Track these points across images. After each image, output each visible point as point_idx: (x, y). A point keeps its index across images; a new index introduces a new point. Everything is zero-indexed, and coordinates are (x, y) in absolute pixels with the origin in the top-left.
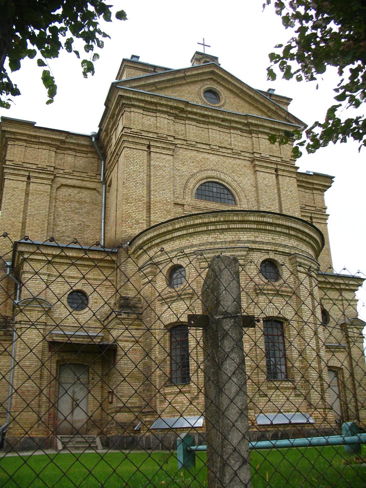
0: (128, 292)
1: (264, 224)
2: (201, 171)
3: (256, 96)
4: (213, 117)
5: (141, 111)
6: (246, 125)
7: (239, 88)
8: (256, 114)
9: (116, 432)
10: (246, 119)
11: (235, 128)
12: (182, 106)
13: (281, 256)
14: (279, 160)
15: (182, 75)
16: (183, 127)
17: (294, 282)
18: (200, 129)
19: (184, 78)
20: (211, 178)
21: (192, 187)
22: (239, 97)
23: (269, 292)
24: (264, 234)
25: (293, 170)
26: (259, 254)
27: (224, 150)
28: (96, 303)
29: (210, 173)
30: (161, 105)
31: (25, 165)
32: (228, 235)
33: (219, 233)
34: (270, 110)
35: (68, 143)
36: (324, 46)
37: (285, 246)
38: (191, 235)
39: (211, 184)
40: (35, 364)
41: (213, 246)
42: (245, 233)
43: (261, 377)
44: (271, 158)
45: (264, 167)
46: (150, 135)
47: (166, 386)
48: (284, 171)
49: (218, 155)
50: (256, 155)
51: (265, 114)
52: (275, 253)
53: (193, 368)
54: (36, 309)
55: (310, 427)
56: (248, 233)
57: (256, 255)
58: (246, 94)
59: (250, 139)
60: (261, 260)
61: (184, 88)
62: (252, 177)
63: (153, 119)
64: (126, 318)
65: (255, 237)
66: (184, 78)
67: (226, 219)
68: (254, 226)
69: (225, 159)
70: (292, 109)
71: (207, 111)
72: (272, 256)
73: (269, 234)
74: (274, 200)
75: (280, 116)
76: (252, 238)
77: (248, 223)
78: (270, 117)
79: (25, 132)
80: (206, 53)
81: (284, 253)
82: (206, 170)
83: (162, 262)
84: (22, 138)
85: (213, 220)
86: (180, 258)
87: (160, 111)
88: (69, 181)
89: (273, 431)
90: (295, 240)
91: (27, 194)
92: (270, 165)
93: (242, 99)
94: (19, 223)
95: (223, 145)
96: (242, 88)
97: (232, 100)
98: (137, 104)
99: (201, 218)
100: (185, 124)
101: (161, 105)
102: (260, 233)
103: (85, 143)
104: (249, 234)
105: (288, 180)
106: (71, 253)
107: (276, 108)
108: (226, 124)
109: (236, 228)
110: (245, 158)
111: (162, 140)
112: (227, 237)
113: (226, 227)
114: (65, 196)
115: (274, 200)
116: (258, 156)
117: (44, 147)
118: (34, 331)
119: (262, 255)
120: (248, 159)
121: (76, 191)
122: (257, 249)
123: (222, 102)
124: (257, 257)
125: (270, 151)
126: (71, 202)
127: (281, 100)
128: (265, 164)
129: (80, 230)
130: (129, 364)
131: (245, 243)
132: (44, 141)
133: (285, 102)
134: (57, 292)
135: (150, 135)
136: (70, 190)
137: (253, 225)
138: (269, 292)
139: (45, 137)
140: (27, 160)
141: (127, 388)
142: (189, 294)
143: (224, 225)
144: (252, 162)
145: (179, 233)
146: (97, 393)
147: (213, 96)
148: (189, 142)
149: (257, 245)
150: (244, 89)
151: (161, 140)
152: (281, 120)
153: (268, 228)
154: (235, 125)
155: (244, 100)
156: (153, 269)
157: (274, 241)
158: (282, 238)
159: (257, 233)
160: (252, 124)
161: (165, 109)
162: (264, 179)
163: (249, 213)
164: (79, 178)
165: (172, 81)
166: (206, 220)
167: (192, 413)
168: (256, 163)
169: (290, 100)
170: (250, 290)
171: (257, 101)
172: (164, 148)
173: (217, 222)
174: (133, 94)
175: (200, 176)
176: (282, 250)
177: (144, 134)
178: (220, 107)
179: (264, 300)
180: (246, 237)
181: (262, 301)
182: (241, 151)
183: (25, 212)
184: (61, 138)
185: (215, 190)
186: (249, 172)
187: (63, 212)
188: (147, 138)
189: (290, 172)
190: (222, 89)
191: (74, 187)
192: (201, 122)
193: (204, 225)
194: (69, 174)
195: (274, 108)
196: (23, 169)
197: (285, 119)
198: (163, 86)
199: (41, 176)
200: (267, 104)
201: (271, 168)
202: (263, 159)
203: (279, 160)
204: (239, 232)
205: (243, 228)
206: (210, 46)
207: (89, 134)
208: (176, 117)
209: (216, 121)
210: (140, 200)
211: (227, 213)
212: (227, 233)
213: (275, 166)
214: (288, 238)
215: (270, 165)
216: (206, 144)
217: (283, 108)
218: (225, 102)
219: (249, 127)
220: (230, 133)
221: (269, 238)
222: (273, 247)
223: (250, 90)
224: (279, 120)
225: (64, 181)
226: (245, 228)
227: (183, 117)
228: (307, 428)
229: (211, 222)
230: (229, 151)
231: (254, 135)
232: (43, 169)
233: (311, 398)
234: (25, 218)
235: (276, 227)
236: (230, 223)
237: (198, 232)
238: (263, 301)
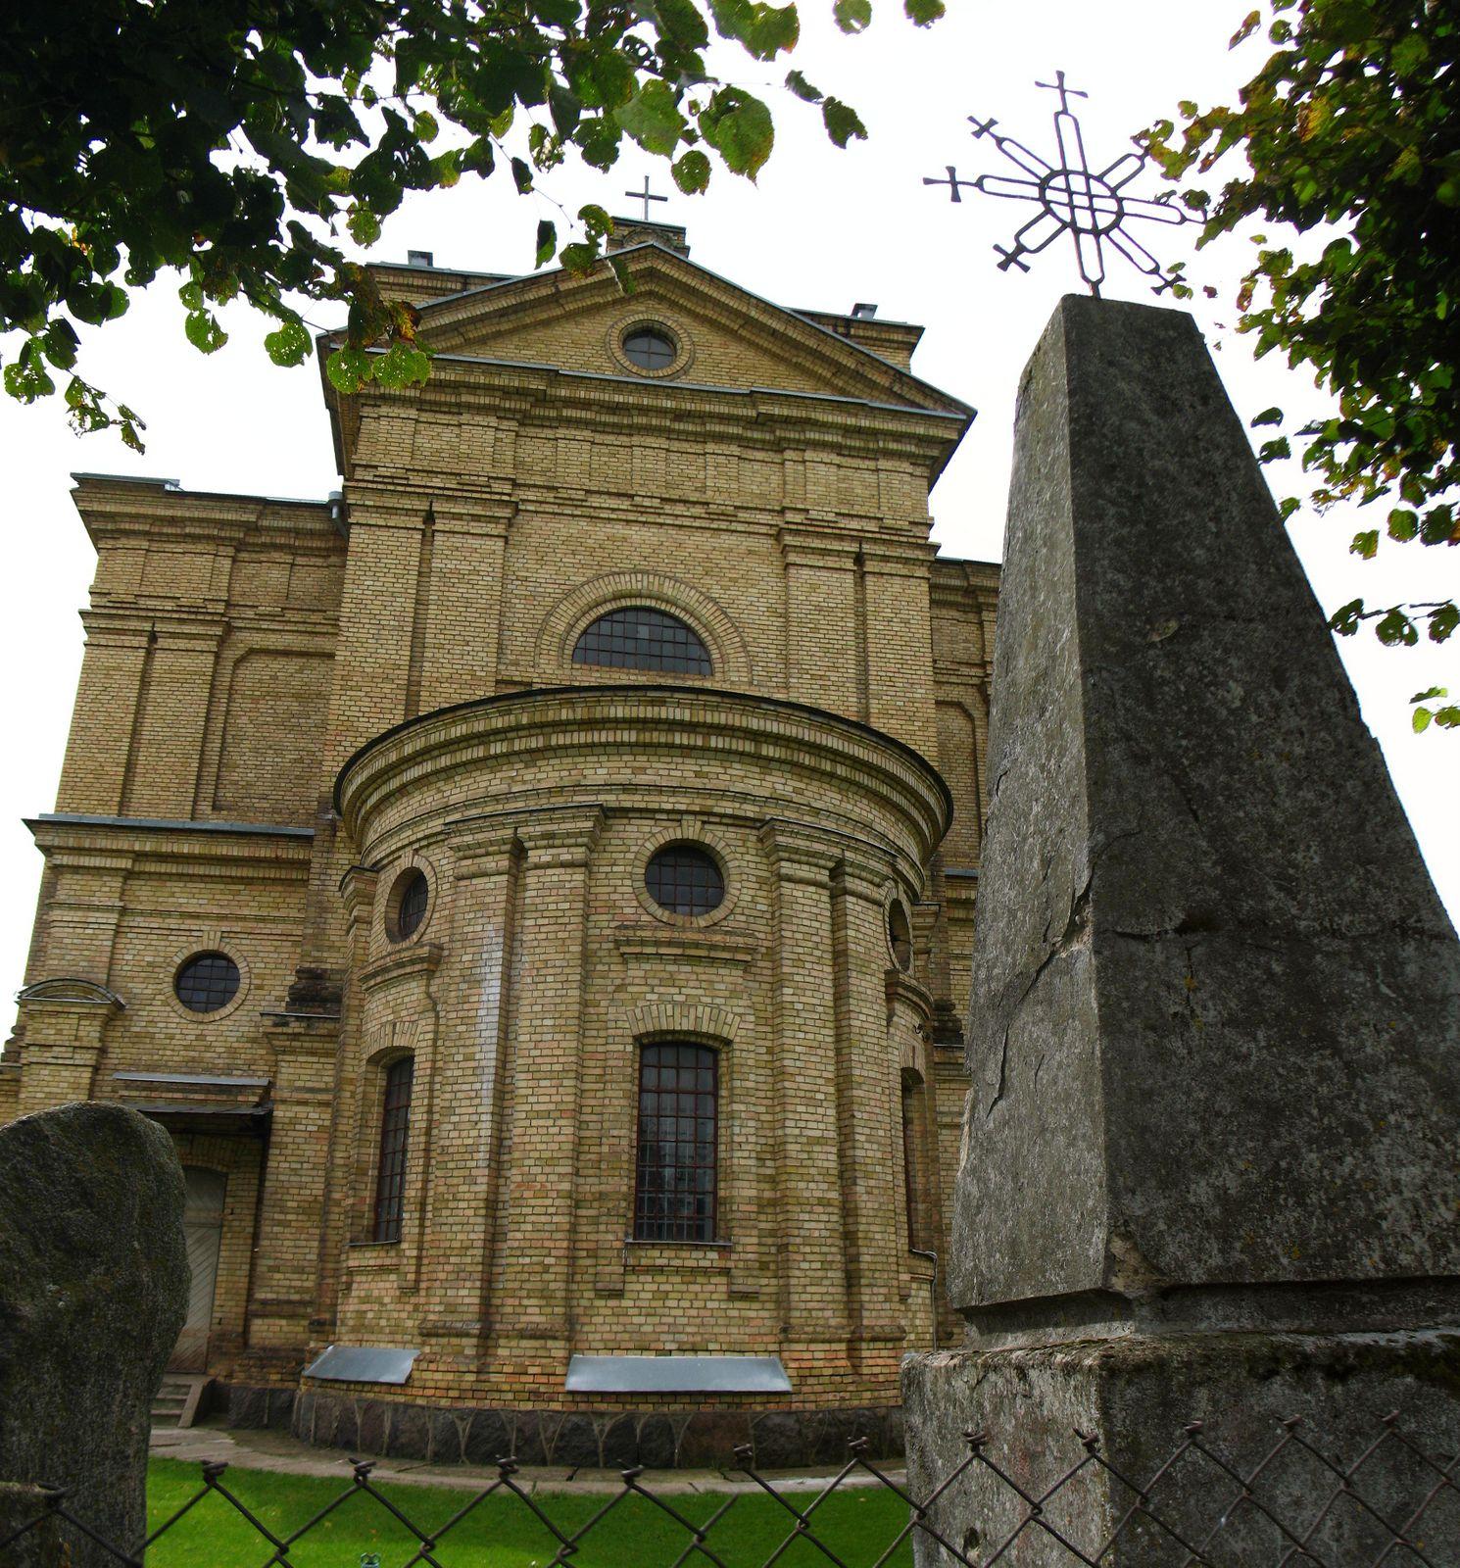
0: (325, 955)
1: (666, 727)
2: (598, 577)
3: (790, 333)
4: (644, 410)
5: (413, 413)
6: (756, 422)
7: (737, 313)
8: (795, 386)
9: (242, 1375)
10: (754, 406)
11: (721, 438)
12: (536, 384)
13: (731, 829)
14: (872, 526)
15: (544, 292)
16: (547, 449)
17: (768, 916)
18: (605, 450)
19: (556, 298)
20: (640, 596)
21: (561, 628)
22: (741, 339)
23: (662, 951)
24: (669, 760)
25: (920, 554)
26: (646, 826)
27: (679, 509)
28: (260, 987)
29: (626, 583)
30: (473, 388)
31: (142, 602)
32: (550, 768)
33: (522, 765)
34: (839, 369)
35: (268, 529)
36: (1390, 223)
37: (745, 797)
38: (448, 773)
39: (631, 617)
41: (500, 807)
42: (604, 758)
43: (607, 1232)
44: (843, 523)
45: (814, 551)
46: (437, 482)
47: (355, 1246)
48: (885, 559)
49: (661, 524)
50: (790, 516)
51: (827, 383)
52: (704, 822)
53: (413, 1193)
54: (73, 1010)
55: (772, 1406)
56: (612, 758)
57: (635, 829)
58: (763, 328)
59: (776, 468)
60: (651, 847)
61: (558, 331)
62: (773, 583)
63: (448, 434)
64: (300, 1034)
65: (635, 771)
66: (556, 298)
67: (538, 718)
68: (629, 736)
69: (681, 536)
70: (923, 365)
71: (621, 392)
72: (691, 830)
73: (687, 761)
74: (842, 652)
75: (873, 385)
76: (625, 776)
77: (607, 725)
78: (842, 392)
79: (142, 511)
80: (652, 219)
81: (738, 821)
82: (614, 574)
83: (385, 862)
84: (137, 527)
85: (499, 723)
86: (421, 848)
87: (469, 407)
88: (273, 637)
89: (616, 1414)
90: (789, 776)
91: (145, 682)
92: (836, 546)
93: (751, 344)
94: (118, 765)
95: (674, 494)
96: (744, 310)
98: (893, 446)
99: (465, 719)
100: (556, 439)
101: (473, 388)
102: (652, 758)
103: (318, 526)
104: (615, 762)
105: (897, 589)
106: (236, 848)
107: (859, 362)
108: (690, 428)
109: (572, 746)
110: (751, 528)
111: (469, 495)
112: (544, 775)
114: (260, 681)
115: (842, 652)
116: (799, 518)
117: (200, 548)
118: (64, 1073)
119: (655, 830)
120: (764, 530)
121: (293, 664)
122: (640, 810)
123: (682, 360)
124: (641, 835)
125: (841, 502)
126: (277, 697)
127: (884, 336)
128: (817, 543)
129: (297, 777)
130: (303, 1172)
131: (598, 793)
132: (198, 531)
133: (897, 342)
134: (147, 959)
135: (437, 482)
136: (276, 665)
137: (626, 733)
138: (662, 951)
139: (201, 520)
140: (151, 589)
141: (292, 1243)
142: (422, 960)
143: (534, 739)
144: (778, 536)
145: (415, 772)
146: (239, 1254)
147: (657, 346)
148: (563, 494)
149: (639, 798)
150: (753, 313)
151: (475, 495)
152: (886, 402)
153: (679, 739)
154: (718, 428)
155: (758, 347)
156: (362, 886)
157: (698, 783)
158: (737, 769)
159: (645, 758)
161: (485, 400)
162: (814, 588)
163: (609, 695)
164: (302, 628)
165: (516, 312)
166: (480, 726)
168: (788, 539)
169: (917, 331)
170: (605, 946)
171: (797, 346)
172: (476, 518)
173: (511, 729)
175: (591, 594)
176: (729, 811)
177: (415, 479)
178: (672, 377)
179: (645, 978)
180: (605, 771)
181: (637, 981)
182: (736, 507)
183: (135, 732)
184: (245, 517)
185: (644, 632)
186: (765, 569)
187: (250, 730)
188: (421, 490)
189: (906, 561)
190: (685, 320)
191: (286, 653)
192: (758, 446)
193: (476, 741)
194: (272, 618)
195: (851, 363)
196: (134, 613)
197: (890, 392)
198: (485, 330)
199: (186, 629)
200: (827, 351)
201: (839, 553)
202: (814, 528)
203: (872, 526)
204: (582, 759)
205: (593, 745)
206: (628, 194)
207: (324, 498)
208: (525, 420)
209: (654, 422)
210: (386, 679)
211: (539, 698)
212: (545, 762)
213: (854, 547)
214: (758, 770)
215: (836, 546)
216: (618, 495)
217: (880, 358)
218: (693, 360)
220: (705, 454)
221: (686, 774)
222: (697, 801)
223: (772, 316)
224: (881, 401)
225: (257, 640)
227: (549, 418)
228: (759, 1408)
229: (496, 732)
230: (698, 510)
231: (789, 454)
232: (194, 610)
233: (793, 1305)
234: (132, 751)
235: (709, 734)
236: (550, 730)
237: (464, 764)
238: (643, 982)
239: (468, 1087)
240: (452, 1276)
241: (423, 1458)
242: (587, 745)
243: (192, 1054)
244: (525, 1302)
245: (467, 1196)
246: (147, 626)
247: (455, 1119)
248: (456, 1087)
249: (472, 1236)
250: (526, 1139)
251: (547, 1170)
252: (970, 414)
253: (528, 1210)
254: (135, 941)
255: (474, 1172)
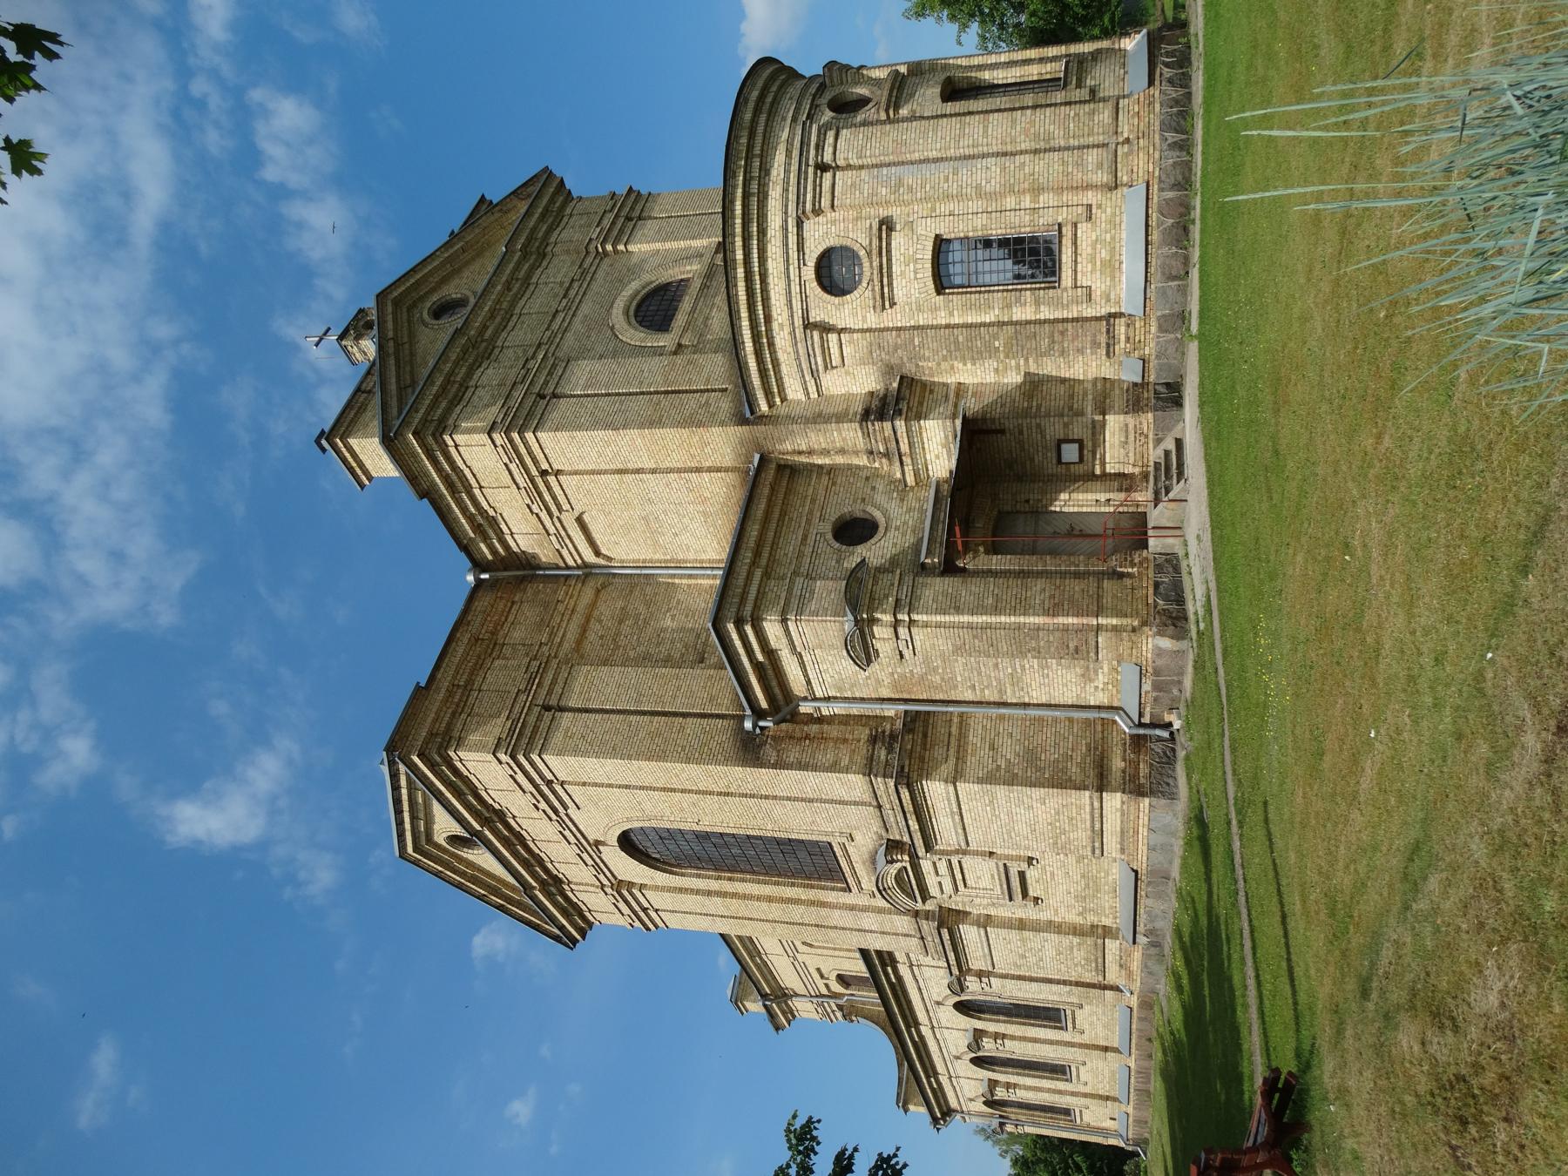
40: (991, 589)
68: (763, 118)
78: (529, 196)
97: (464, 281)
100: (502, 347)
113: (758, 160)
126: (618, 634)
129: (687, 616)
160: (525, 246)
167: (1118, 219)
172: (550, 374)
174: (417, 412)
219: (536, 239)
226: (765, 130)
230: (576, 285)
239: (965, 177)
240: (1080, 168)
241: (1191, 162)
242: (764, 136)
243: (909, 532)
244: (1096, 122)
245: (1032, 167)
246: (537, 710)
247: (984, 183)
248: (964, 185)
249: (1056, 159)
250: (999, 136)
251: (1018, 122)
252: (547, 174)
253: (1042, 129)
254: (819, 572)
255: (1017, 164)
